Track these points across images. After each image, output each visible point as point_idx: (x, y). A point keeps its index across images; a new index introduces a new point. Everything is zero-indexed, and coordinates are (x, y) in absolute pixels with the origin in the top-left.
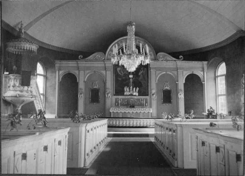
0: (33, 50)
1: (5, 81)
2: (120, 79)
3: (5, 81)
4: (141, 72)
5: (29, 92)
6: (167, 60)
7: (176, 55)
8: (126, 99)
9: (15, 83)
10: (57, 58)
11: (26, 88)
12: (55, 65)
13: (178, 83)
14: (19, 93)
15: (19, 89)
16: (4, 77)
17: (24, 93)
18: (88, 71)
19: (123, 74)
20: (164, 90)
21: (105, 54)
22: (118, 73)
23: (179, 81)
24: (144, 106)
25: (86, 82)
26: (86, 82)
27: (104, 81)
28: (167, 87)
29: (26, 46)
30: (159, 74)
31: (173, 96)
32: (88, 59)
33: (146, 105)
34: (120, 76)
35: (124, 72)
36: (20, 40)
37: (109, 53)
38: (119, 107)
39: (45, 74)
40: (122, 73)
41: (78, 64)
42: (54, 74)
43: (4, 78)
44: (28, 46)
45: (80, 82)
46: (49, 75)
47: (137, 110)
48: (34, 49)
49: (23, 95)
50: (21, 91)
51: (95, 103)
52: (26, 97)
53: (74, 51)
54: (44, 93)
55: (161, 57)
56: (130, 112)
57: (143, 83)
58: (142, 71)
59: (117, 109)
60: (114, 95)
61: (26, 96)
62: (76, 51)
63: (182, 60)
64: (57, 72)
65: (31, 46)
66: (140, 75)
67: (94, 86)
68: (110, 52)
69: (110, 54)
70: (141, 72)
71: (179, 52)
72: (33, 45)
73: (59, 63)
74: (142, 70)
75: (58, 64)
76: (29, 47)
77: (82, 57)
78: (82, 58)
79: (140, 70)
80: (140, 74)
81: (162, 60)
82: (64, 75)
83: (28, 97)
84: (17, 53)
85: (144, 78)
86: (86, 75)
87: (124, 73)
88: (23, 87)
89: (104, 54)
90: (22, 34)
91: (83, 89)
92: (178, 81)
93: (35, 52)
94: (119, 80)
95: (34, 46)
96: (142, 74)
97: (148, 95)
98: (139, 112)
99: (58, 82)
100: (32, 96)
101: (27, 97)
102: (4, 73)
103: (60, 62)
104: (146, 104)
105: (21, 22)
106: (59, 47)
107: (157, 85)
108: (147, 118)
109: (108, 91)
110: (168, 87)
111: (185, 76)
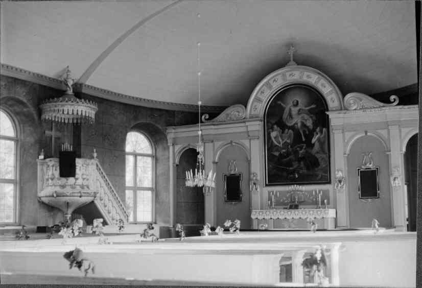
0: (84, 114)
1: (42, 170)
2: (277, 154)
3: (42, 170)
4: (317, 136)
5: (85, 187)
6: (363, 108)
7: (383, 97)
8: (288, 192)
9: (54, 172)
10: (170, 124)
11: (71, 180)
12: (166, 137)
13: (390, 154)
14: (58, 189)
15: (60, 183)
16: (38, 164)
17: (68, 190)
18: (220, 143)
19: (281, 144)
20: (362, 170)
21: (246, 107)
22: (272, 141)
23: (392, 149)
24: (320, 206)
25: (219, 164)
26: (217, 163)
27: (247, 159)
28: (368, 165)
29: (81, 110)
30: (408, 133)
31: (381, 180)
32: (218, 120)
33: (323, 203)
34: (278, 149)
35: (283, 140)
36: (67, 99)
37: (254, 106)
38: (319, 208)
39: (154, 154)
40: (281, 140)
41: (247, 126)
42: (166, 153)
43: (40, 165)
44: (79, 109)
45: (252, 160)
46: (160, 153)
47: (300, 214)
48: (89, 112)
49: (63, 193)
50: (63, 187)
51: (233, 203)
52: (67, 196)
53: (188, 105)
54: (154, 187)
55: (352, 102)
56: (280, 218)
57: (320, 160)
58: (319, 135)
59: (263, 213)
60: (266, 185)
61: (68, 194)
62: (214, 107)
63: (397, 105)
64: (171, 148)
65: (76, 107)
66: (314, 144)
67: (231, 170)
68: (255, 104)
69: (256, 106)
70: (317, 136)
71: (388, 92)
72: (79, 105)
73: (173, 131)
74: (317, 134)
75: (172, 133)
76: (73, 110)
77: (207, 117)
78: (208, 120)
79: (315, 133)
80: (314, 140)
81: (355, 109)
82: (181, 154)
83: (73, 196)
84: (66, 121)
85: (323, 151)
86: (217, 151)
87: (284, 141)
88: (67, 180)
89: (244, 107)
90: (68, 89)
91: (259, 175)
92: (390, 151)
93: (91, 118)
94: (275, 156)
95: (82, 107)
96: (319, 140)
97: (329, 183)
98: (304, 217)
99: (173, 166)
100: (79, 195)
101: (70, 196)
102: (38, 158)
103: (174, 129)
104: (325, 201)
105: (68, 67)
106: (172, 103)
107: (349, 158)
108: (298, 229)
109: (254, 178)
110: (370, 164)
111: (404, 138)
